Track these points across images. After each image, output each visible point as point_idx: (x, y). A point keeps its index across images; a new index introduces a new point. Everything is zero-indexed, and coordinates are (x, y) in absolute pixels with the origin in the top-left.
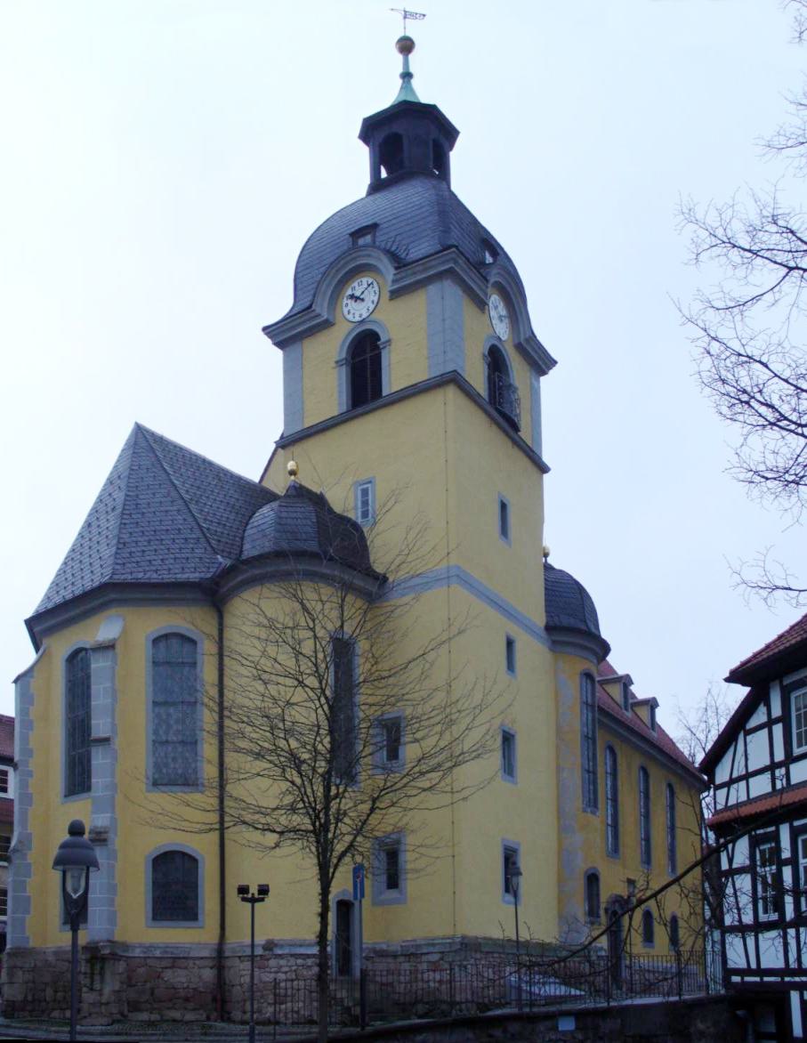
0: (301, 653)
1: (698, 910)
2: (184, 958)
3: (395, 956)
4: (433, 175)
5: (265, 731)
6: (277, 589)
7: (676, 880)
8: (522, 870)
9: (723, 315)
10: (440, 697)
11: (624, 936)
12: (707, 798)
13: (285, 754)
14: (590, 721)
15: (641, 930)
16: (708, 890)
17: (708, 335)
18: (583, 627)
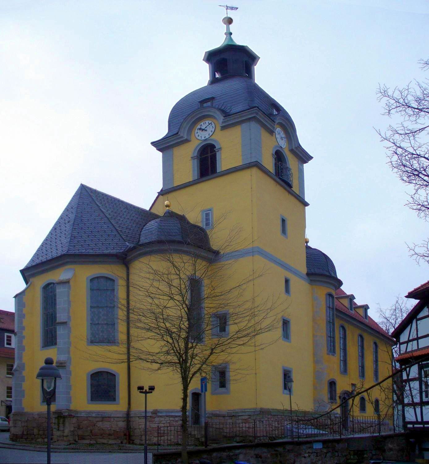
0: (173, 285)
1: (390, 397)
2: (109, 417)
3: (224, 417)
6: (159, 257)
7: (379, 384)
8: (293, 380)
9: (404, 137)
10: (248, 305)
11: (350, 408)
12: (396, 348)
13: (164, 329)
14: (331, 316)
15: (359, 405)
16: (395, 388)
17: (396, 146)
18: (328, 274)
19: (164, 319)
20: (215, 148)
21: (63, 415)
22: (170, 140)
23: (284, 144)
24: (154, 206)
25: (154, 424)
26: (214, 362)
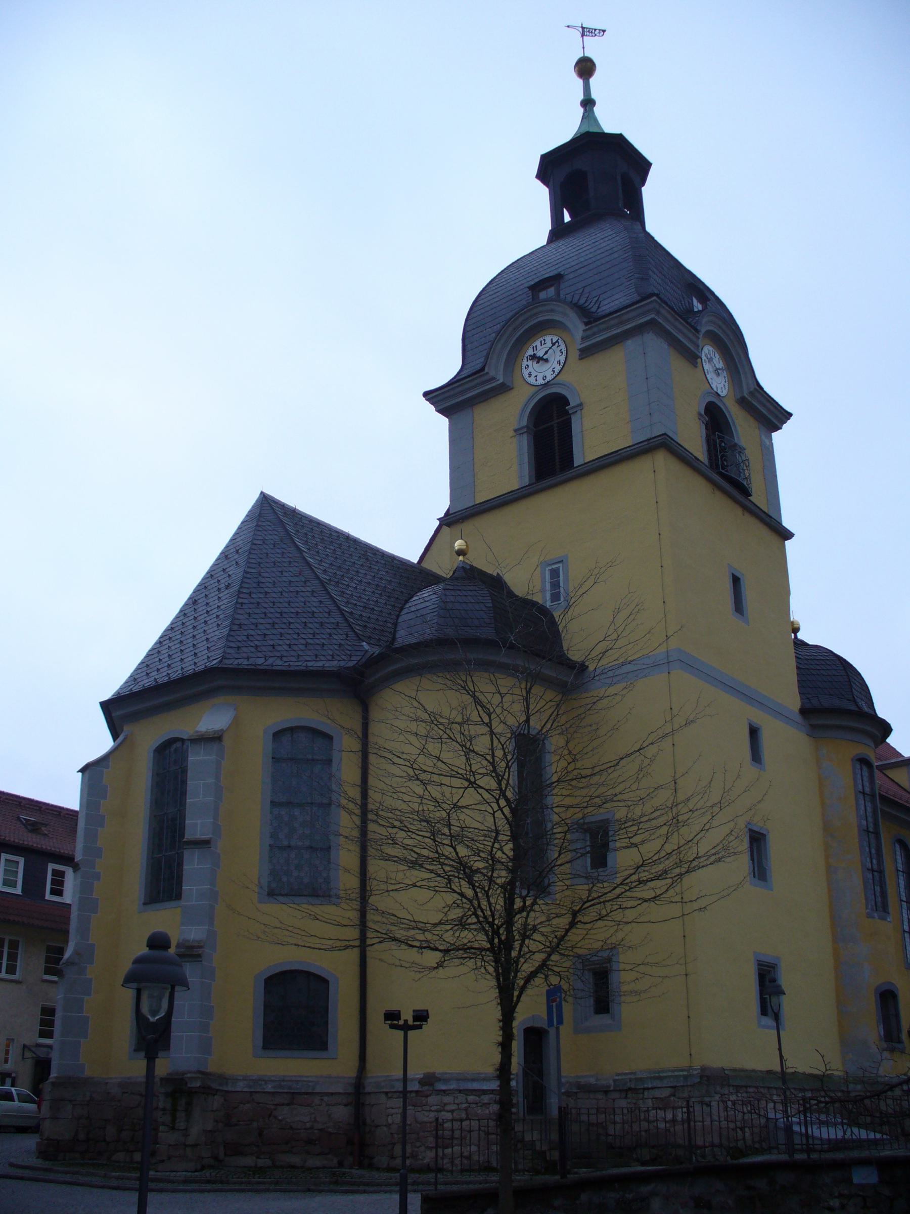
0: (473, 751)
2: (307, 1094)
4: (624, 216)
5: (424, 837)
6: (441, 681)
8: (785, 987)
10: (664, 797)
13: (451, 863)
14: (869, 814)
18: (853, 707)
19: (453, 837)
20: (569, 404)
21: (189, 1086)
22: (466, 386)
23: (724, 385)
24: (429, 552)
25: (426, 1114)
26: (579, 945)
